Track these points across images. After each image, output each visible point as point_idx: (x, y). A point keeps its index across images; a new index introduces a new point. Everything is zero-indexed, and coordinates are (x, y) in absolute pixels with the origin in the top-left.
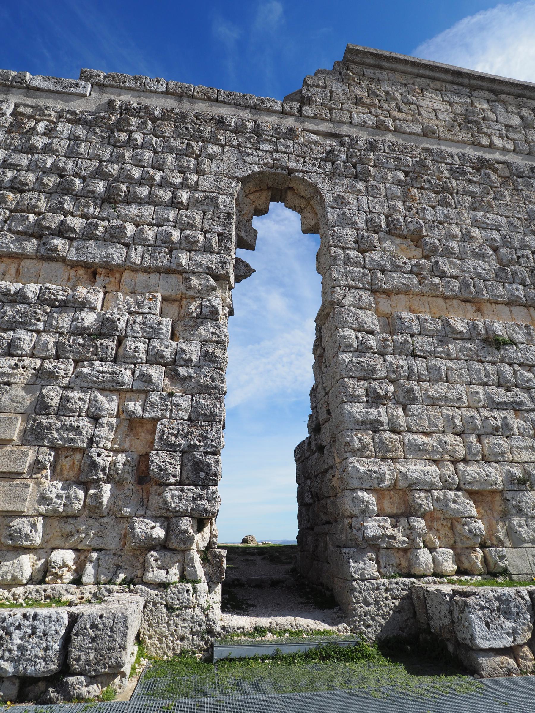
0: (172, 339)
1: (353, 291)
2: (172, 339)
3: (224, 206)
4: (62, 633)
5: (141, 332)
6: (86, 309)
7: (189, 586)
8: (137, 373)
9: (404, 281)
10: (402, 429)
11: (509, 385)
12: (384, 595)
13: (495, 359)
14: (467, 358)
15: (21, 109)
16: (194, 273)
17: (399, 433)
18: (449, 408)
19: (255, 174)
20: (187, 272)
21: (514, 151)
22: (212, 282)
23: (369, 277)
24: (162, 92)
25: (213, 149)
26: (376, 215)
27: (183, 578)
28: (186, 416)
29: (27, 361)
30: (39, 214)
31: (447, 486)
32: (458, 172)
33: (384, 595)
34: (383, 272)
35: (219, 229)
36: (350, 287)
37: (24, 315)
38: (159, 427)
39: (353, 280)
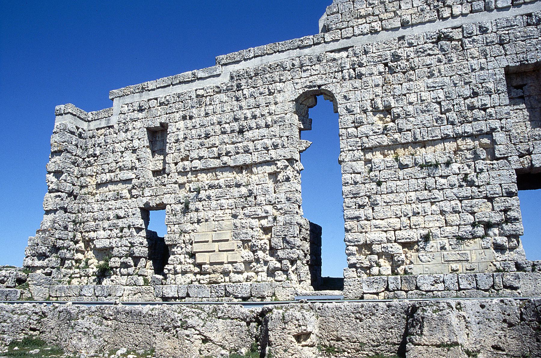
0: (275, 193)
1: (351, 152)
2: (275, 193)
3: (288, 120)
4: (216, 166)
5: (262, 192)
6: (214, 173)
7: (289, 281)
8: (263, 210)
9: (378, 140)
10: (370, 219)
11: (430, 189)
12: (357, 283)
13: (425, 176)
14: (409, 178)
15: (198, 93)
16: (279, 160)
17: (370, 220)
18: (395, 206)
19: (301, 95)
20: (276, 161)
21: (471, 12)
22: (287, 164)
23: (360, 143)
24: (252, 57)
25: (280, 86)
26: (365, 101)
27: (288, 279)
28: (282, 224)
29: (227, 211)
30: (217, 147)
31: (389, 241)
32: (420, 51)
33: (357, 283)
34: (367, 137)
35: (287, 134)
36: (349, 151)
37: (221, 193)
38: (273, 229)
39: (351, 146)
